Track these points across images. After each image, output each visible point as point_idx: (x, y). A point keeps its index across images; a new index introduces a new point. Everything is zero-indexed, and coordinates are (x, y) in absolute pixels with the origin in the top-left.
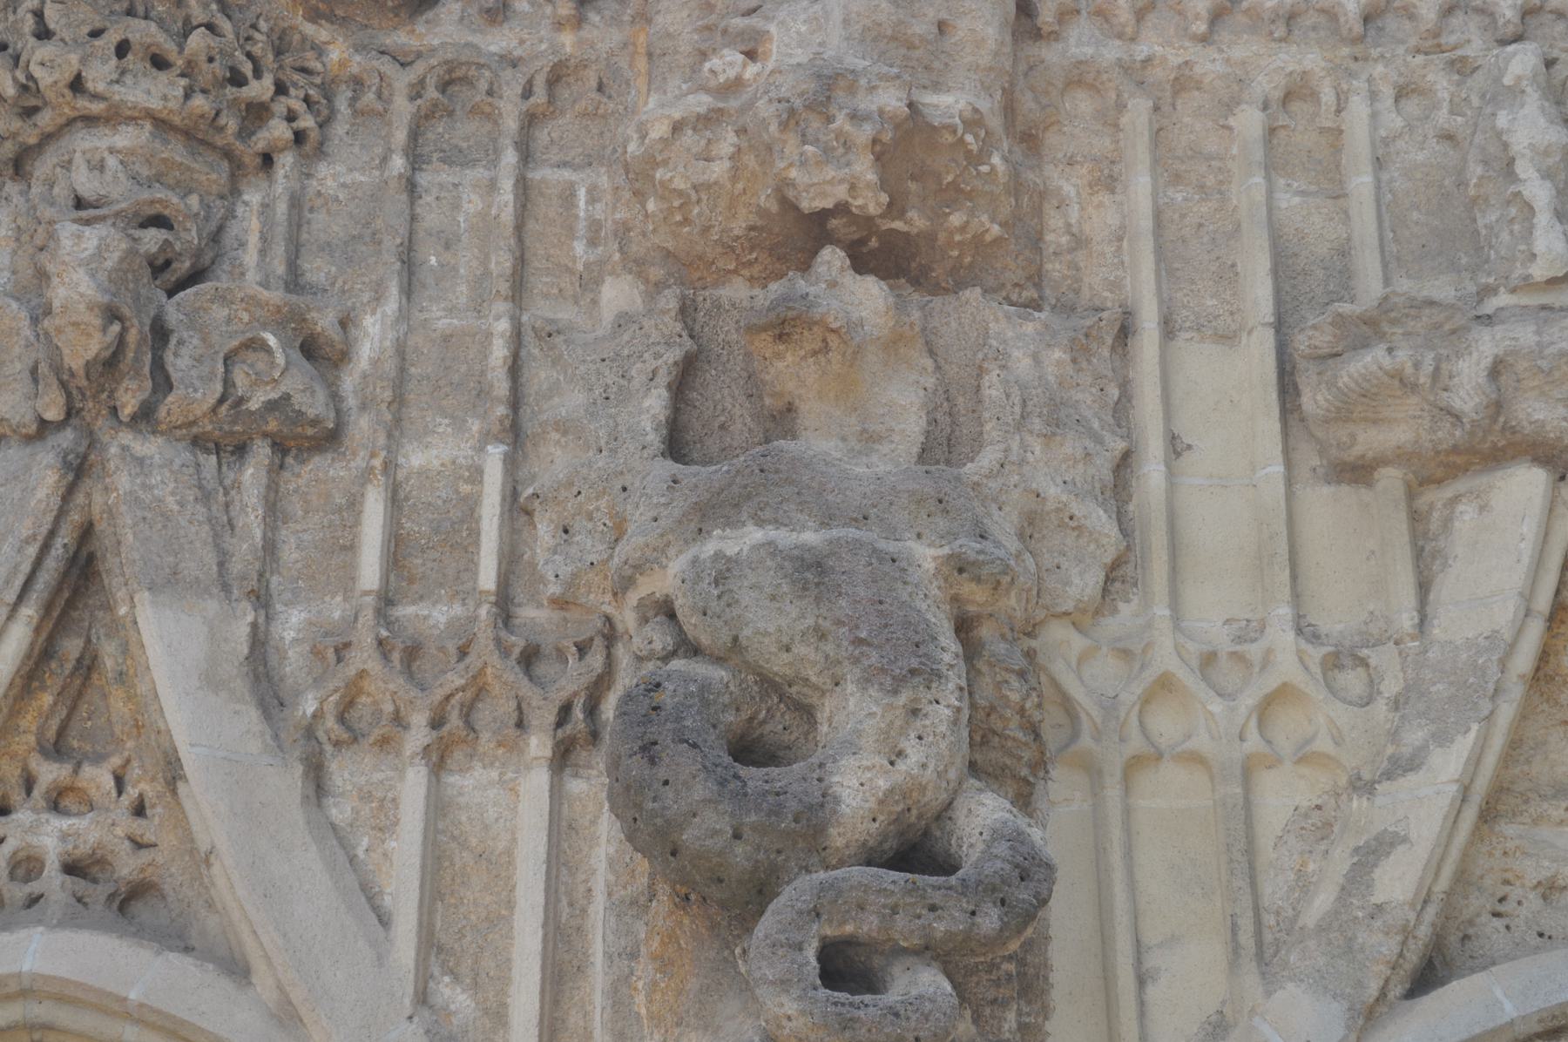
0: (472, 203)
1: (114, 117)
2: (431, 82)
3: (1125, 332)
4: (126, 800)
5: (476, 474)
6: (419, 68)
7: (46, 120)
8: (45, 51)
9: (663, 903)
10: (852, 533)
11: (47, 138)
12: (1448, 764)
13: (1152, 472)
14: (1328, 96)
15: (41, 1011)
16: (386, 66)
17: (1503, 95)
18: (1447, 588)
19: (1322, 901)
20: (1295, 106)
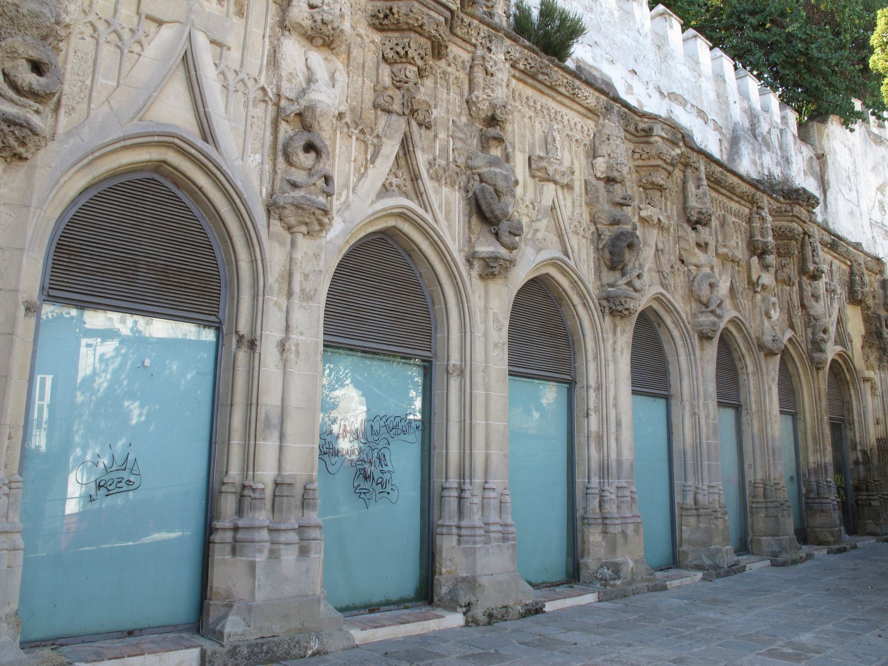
11: (401, 62)
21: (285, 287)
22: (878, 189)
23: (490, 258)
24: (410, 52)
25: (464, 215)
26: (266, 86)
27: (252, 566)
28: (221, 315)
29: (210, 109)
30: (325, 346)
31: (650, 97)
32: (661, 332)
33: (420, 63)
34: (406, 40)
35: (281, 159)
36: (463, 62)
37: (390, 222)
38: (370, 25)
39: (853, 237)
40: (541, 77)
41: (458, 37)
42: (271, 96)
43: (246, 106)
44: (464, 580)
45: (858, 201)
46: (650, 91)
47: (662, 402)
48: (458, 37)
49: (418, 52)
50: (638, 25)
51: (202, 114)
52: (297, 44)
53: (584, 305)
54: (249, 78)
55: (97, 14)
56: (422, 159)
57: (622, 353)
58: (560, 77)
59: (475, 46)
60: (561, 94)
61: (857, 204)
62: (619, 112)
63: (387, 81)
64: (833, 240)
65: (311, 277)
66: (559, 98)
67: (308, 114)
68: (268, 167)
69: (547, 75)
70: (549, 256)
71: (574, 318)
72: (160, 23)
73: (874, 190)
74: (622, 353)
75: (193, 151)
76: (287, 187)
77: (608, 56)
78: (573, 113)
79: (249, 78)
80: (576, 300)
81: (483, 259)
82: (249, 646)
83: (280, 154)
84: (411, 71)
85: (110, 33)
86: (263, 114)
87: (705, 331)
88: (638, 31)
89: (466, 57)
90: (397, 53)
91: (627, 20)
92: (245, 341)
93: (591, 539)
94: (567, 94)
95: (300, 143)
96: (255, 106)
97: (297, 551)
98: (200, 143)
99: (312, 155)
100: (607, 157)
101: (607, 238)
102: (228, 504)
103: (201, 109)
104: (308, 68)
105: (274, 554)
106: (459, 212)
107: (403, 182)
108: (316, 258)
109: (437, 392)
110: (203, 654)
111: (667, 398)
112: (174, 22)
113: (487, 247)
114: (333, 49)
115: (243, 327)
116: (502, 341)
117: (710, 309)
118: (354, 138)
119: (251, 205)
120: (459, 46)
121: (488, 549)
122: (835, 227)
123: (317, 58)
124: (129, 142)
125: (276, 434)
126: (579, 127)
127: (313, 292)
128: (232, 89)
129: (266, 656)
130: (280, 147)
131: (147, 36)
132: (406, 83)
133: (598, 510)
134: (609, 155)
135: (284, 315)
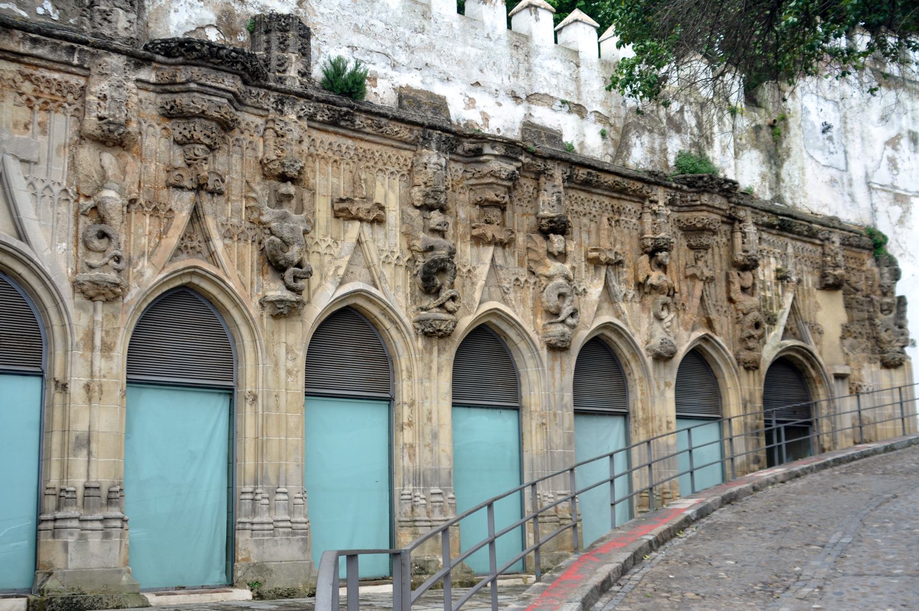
1: (202, 143)
21: (90, 342)
22: (887, 143)
24: (195, 134)
25: (258, 264)
27: (66, 545)
28: (43, 366)
29: (22, 216)
30: (127, 382)
31: (500, 105)
32: (509, 344)
33: (207, 141)
34: (192, 125)
35: (81, 245)
36: (257, 126)
37: (185, 280)
39: (830, 211)
40: (343, 123)
43: (52, 206)
45: (847, 163)
46: (499, 100)
47: (514, 413)
50: (488, 30)
51: (16, 220)
52: (92, 150)
53: (397, 328)
56: (211, 223)
57: (439, 370)
59: (268, 110)
60: (368, 134)
61: (843, 167)
62: (439, 141)
63: (179, 162)
64: (782, 220)
65: (111, 333)
67: (100, 208)
68: (72, 252)
70: (357, 288)
73: (878, 146)
74: (439, 370)
75: (11, 250)
76: (86, 268)
77: (442, 75)
78: (386, 148)
80: (388, 325)
81: (272, 302)
82: (62, 598)
83: (80, 241)
84: (200, 150)
86: (66, 211)
87: (553, 342)
88: (488, 37)
89: (260, 121)
90: (185, 136)
91: (473, 27)
92: (59, 385)
93: (402, 539)
95: (93, 232)
96: (59, 204)
97: (101, 536)
98: (16, 243)
99: (105, 240)
100: (423, 186)
101: (421, 264)
102: (50, 503)
103: (15, 216)
104: (102, 167)
105: (83, 538)
106: (252, 263)
109: (237, 414)
110: (28, 601)
111: (625, 415)
113: (276, 291)
115: (58, 375)
117: (560, 319)
119: (57, 284)
121: (276, 541)
122: (797, 202)
123: (108, 159)
124: (36, 62)
125: (85, 452)
126: (394, 159)
128: (39, 195)
130: (80, 236)
132: (195, 160)
133: (409, 514)
134: (425, 183)
135: (89, 363)
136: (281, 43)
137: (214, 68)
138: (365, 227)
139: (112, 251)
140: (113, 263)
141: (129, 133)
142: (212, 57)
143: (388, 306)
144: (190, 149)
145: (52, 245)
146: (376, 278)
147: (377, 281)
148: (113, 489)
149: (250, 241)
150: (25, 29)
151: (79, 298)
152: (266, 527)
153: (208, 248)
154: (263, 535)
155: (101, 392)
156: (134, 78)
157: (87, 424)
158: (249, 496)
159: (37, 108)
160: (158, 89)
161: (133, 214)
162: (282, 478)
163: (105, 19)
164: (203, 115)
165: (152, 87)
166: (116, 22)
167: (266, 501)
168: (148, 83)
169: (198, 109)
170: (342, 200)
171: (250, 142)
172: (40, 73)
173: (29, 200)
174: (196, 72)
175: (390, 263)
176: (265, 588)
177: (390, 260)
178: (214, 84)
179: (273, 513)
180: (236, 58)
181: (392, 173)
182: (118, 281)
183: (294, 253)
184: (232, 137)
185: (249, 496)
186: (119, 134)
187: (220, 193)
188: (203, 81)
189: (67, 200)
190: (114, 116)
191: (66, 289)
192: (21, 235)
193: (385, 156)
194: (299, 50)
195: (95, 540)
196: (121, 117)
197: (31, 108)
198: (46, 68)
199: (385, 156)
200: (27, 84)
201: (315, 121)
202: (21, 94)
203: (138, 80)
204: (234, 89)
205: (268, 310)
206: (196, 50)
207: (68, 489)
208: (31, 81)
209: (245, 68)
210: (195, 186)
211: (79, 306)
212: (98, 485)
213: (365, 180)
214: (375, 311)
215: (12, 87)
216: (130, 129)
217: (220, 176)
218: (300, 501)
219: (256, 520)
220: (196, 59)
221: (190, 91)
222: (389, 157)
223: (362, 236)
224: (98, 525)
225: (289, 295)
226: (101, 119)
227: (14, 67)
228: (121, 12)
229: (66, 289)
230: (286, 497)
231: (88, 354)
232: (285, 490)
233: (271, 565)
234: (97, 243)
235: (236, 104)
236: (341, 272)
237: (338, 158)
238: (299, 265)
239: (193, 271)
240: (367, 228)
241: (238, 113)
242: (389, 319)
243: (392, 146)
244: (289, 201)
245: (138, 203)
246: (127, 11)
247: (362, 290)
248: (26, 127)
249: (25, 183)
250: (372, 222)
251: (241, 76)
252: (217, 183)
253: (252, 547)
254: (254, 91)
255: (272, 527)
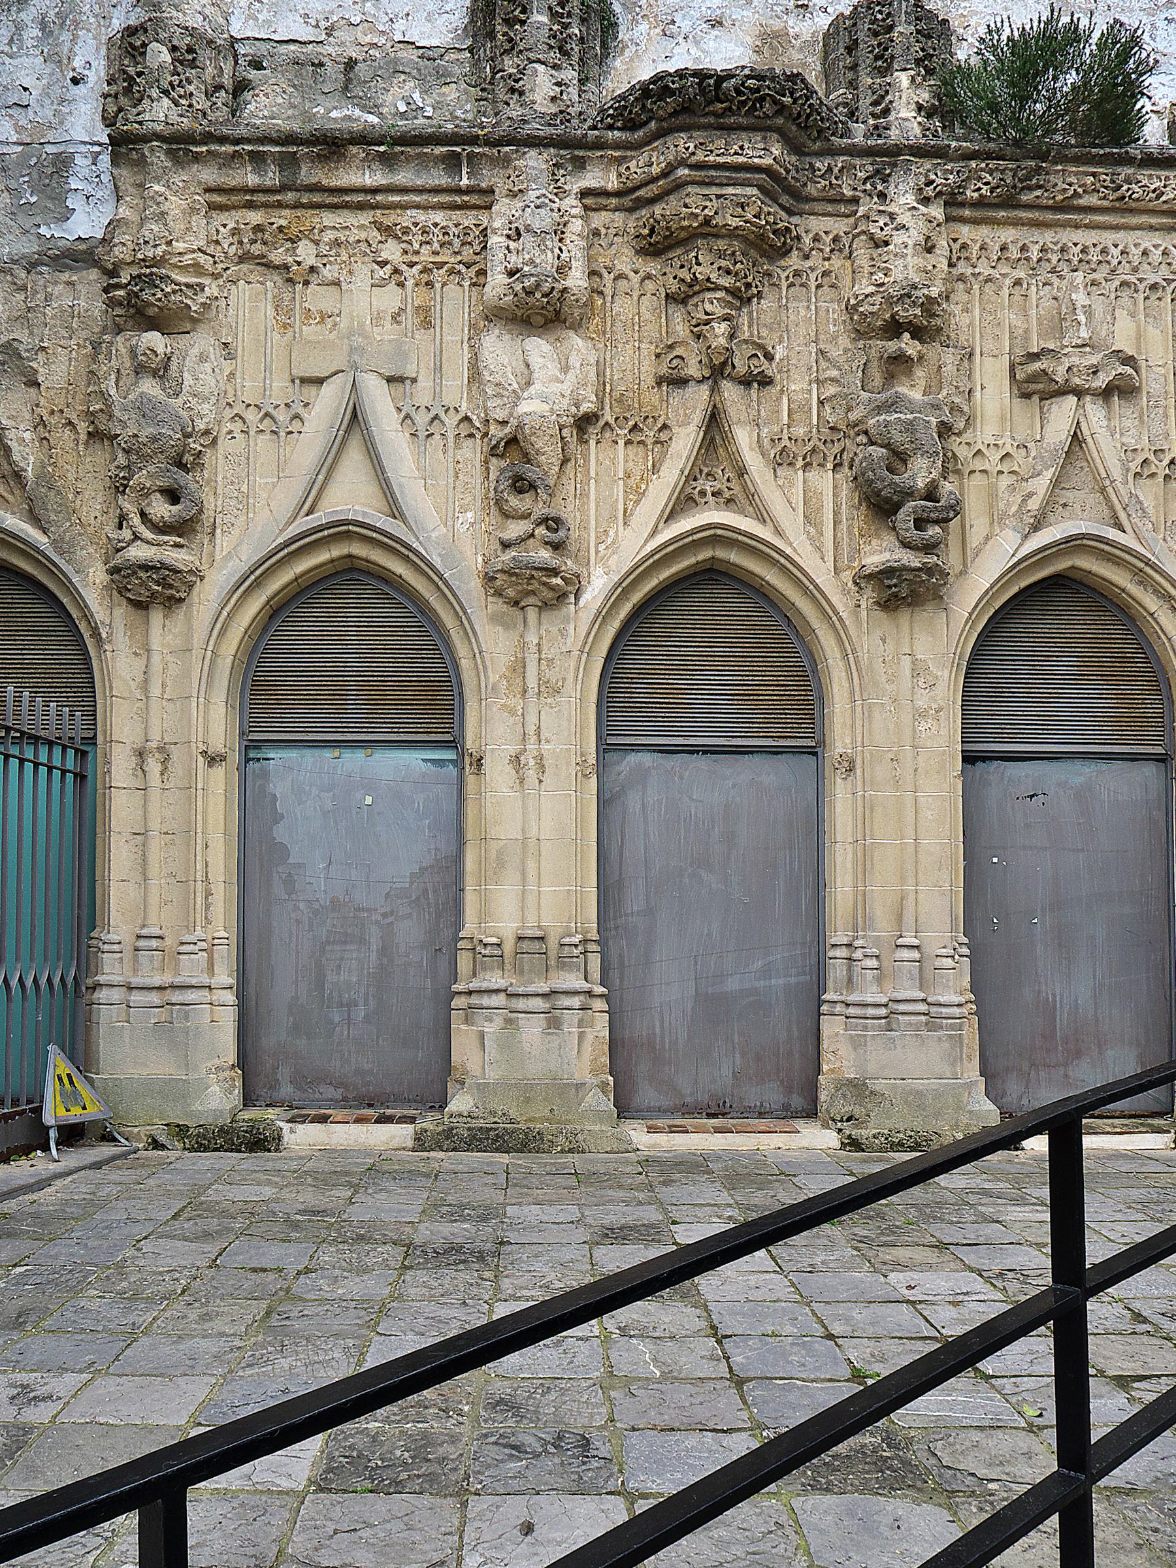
0: (803, 312)
1: (717, 288)
2: (791, 276)
3: (971, 355)
4: (725, 478)
5: (810, 391)
6: (788, 271)
7: (697, 288)
8: (700, 269)
9: (864, 507)
10: (918, 415)
11: (695, 294)
12: (1049, 474)
13: (978, 394)
14: (1025, 286)
15: (719, 532)
16: (779, 270)
17: (1074, 287)
18: (1047, 428)
19: (1014, 508)
20: (1016, 287)
23: (881, 572)
26: (469, 414)
33: (726, 281)
37: (704, 554)
38: (638, 252)
40: (1025, 198)
41: (814, 200)
42: (478, 426)
44: (850, 1082)
48: (814, 200)
49: (715, 266)
54: (446, 412)
55: (243, 402)
56: (743, 437)
58: (1073, 179)
63: (681, 330)
66: (1089, 218)
69: (1040, 187)
71: (1159, 638)
72: (320, 381)
79: (446, 412)
84: (713, 304)
85: (261, 420)
86: (472, 452)
94: (1106, 203)
96: (457, 446)
97: (544, 1024)
107: (727, 484)
108: (562, 635)
112: (335, 373)
114: (564, 322)
116: (934, 706)
118: (621, 443)
119: (454, 584)
120: (824, 215)
127: (560, 683)
129: (492, 1143)
131: (306, 405)
136: (877, 58)
137: (722, 128)
138: (1089, 407)
139: (540, 510)
140: (541, 531)
141: (565, 290)
142: (710, 103)
143: (1148, 563)
144: (696, 305)
145: (448, 520)
146: (1118, 507)
147: (1122, 516)
148: (566, 940)
149: (830, 466)
150: (363, 139)
151: (498, 606)
152: (871, 1011)
153: (745, 488)
154: (865, 1028)
155: (542, 768)
156: (576, 189)
157: (520, 827)
158: (842, 952)
159: (410, 283)
160: (627, 201)
161: (592, 443)
162: (909, 917)
163: (513, 90)
164: (707, 230)
165: (614, 201)
166: (532, 90)
167: (874, 963)
168: (604, 193)
169: (696, 216)
170: (1034, 357)
171: (825, 274)
172: (406, 219)
173: (405, 445)
174: (682, 144)
175: (1153, 475)
176: (863, 1133)
177: (1153, 469)
178: (721, 160)
179: (888, 985)
180: (758, 90)
181: (1154, 287)
182: (554, 563)
183: (920, 472)
184: (784, 269)
185: (842, 952)
186: (545, 295)
187: (765, 381)
188: (700, 156)
189: (471, 435)
190: (532, 261)
191: (471, 589)
192: (395, 510)
193: (1135, 253)
194: (918, 62)
195: (532, 1030)
196: (547, 261)
197: (401, 285)
198: (417, 207)
199: (1135, 253)
200: (391, 243)
201: (962, 205)
202: (383, 264)
203: (585, 193)
204: (768, 161)
205: (868, 596)
206: (672, 93)
207: (485, 941)
208: (396, 237)
209: (781, 109)
210: (707, 373)
211: (496, 619)
212: (538, 933)
213: (1088, 310)
214: (1119, 577)
215: (365, 254)
216: (569, 283)
217: (761, 347)
218: (949, 962)
219: (851, 998)
220: (675, 113)
221: (679, 186)
222: (1145, 253)
223: (1084, 426)
224: (538, 1004)
225: (912, 559)
226: (511, 273)
227: (365, 218)
228: (541, 68)
229: (471, 589)
230: (915, 955)
231: (516, 702)
232: (915, 942)
233: (878, 1085)
234: (514, 502)
235: (785, 199)
236: (1034, 504)
237: (1022, 275)
238: (931, 494)
239: (716, 536)
240: (1095, 411)
241: (795, 220)
242: (1155, 591)
243: (1151, 228)
244: (909, 373)
245: (601, 423)
246: (555, 67)
247: (1084, 536)
248: (395, 318)
249: (396, 418)
250: (1106, 393)
251: (779, 130)
252: (755, 361)
253: (844, 1050)
254: (821, 165)
255: (883, 1012)
